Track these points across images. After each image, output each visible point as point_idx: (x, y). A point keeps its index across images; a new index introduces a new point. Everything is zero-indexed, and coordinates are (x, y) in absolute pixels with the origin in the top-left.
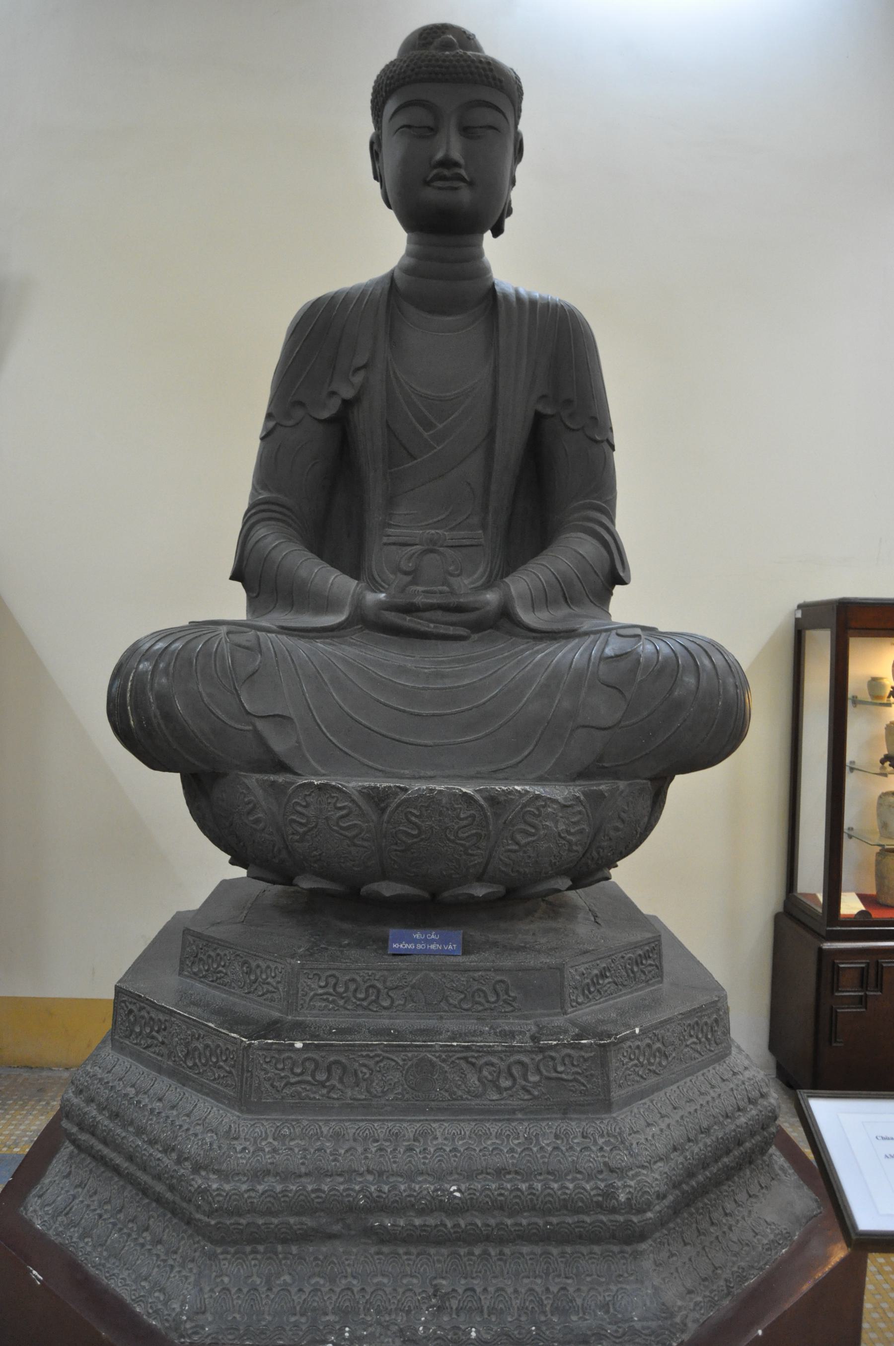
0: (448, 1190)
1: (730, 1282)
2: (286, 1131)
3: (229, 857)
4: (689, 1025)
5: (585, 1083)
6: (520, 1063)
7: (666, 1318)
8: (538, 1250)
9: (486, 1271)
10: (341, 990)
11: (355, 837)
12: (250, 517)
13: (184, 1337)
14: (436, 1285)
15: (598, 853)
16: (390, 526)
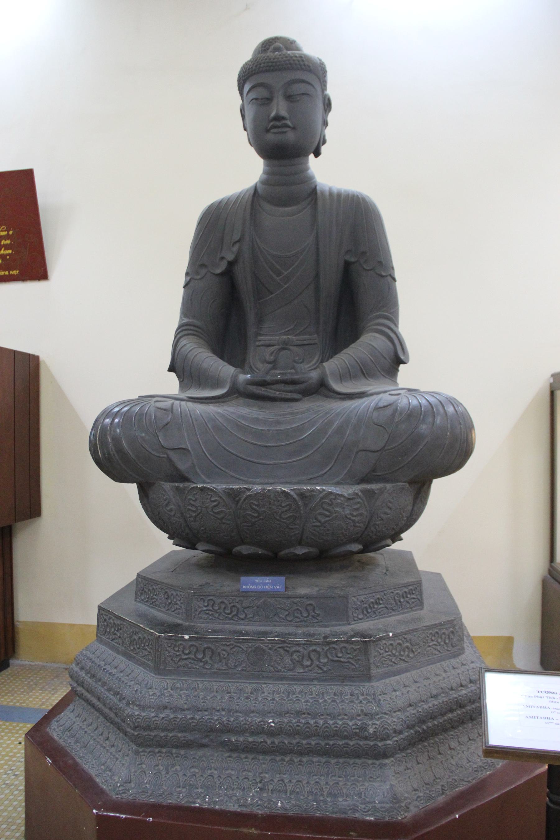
0: (267, 722)
1: (445, 787)
2: (178, 685)
3: (168, 535)
4: (431, 633)
5: (355, 664)
6: (315, 651)
7: (396, 803)
8: (323, 760)
9: (291, 771)
10: (216, 608)
11: (223, 518)
12: (178, 334)
13: (118, 794)
14: (261, 777)
15: (375, 528)
16: (261, 335)
